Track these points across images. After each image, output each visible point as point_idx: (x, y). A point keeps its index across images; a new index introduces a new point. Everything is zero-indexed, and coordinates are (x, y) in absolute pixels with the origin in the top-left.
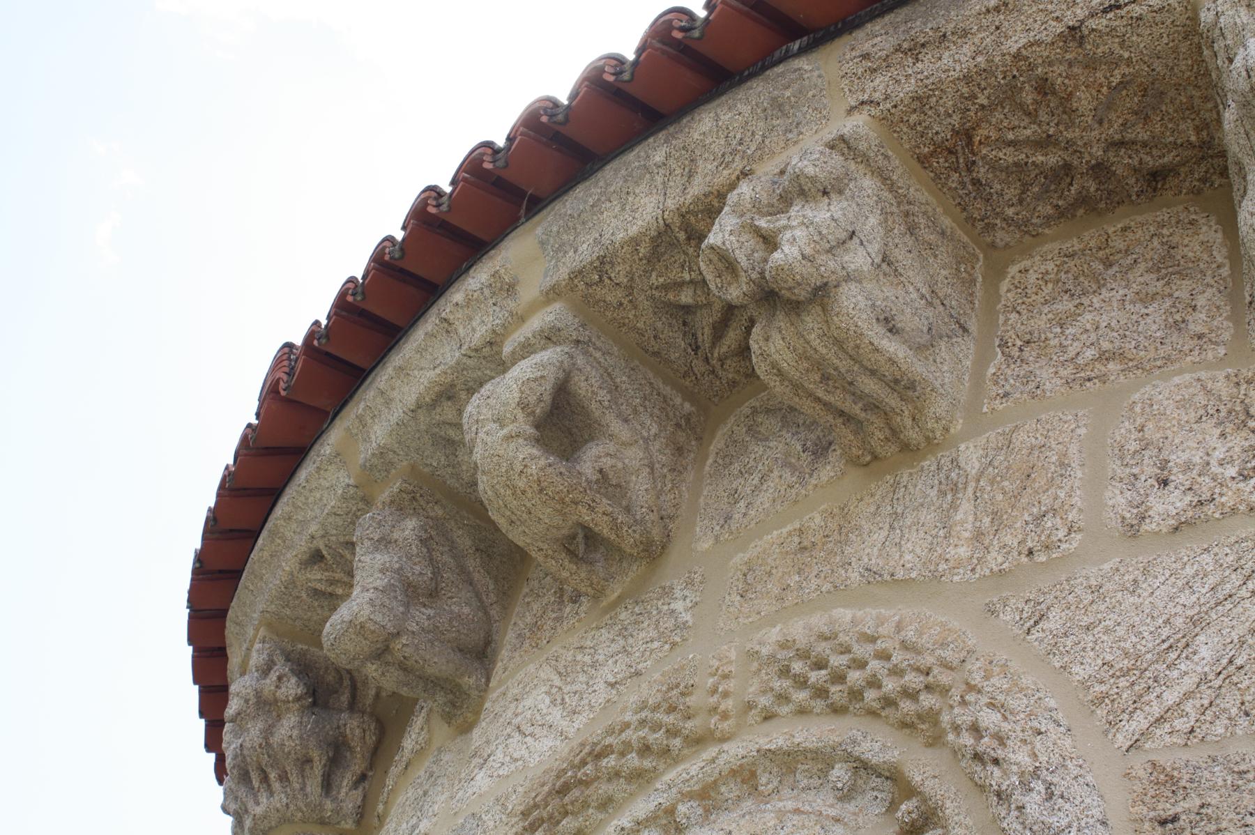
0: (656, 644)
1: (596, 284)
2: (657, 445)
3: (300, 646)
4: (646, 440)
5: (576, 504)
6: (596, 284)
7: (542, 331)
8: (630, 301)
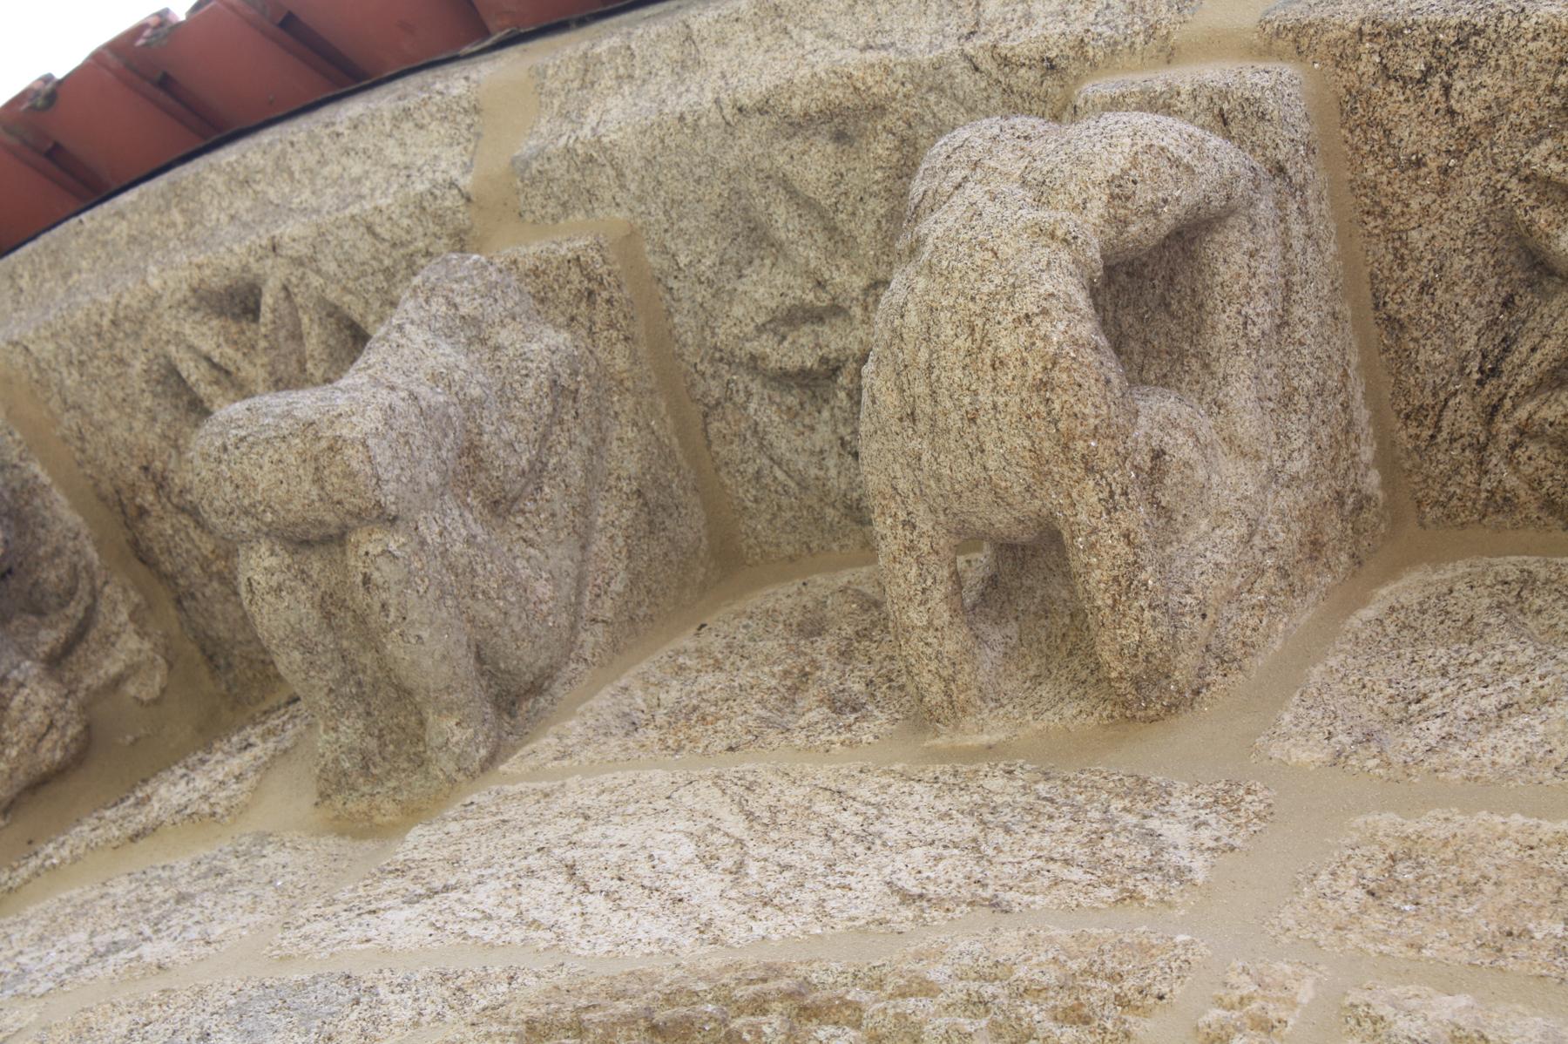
0: (1076, 874)
1: (1405, 82)
2: (1286, 499)
3: (36, 468)
4: (1273, 474)
5: (1089, 470)
6: (1405, 82)
7: (1224, 96)
8: (1445, 171)
